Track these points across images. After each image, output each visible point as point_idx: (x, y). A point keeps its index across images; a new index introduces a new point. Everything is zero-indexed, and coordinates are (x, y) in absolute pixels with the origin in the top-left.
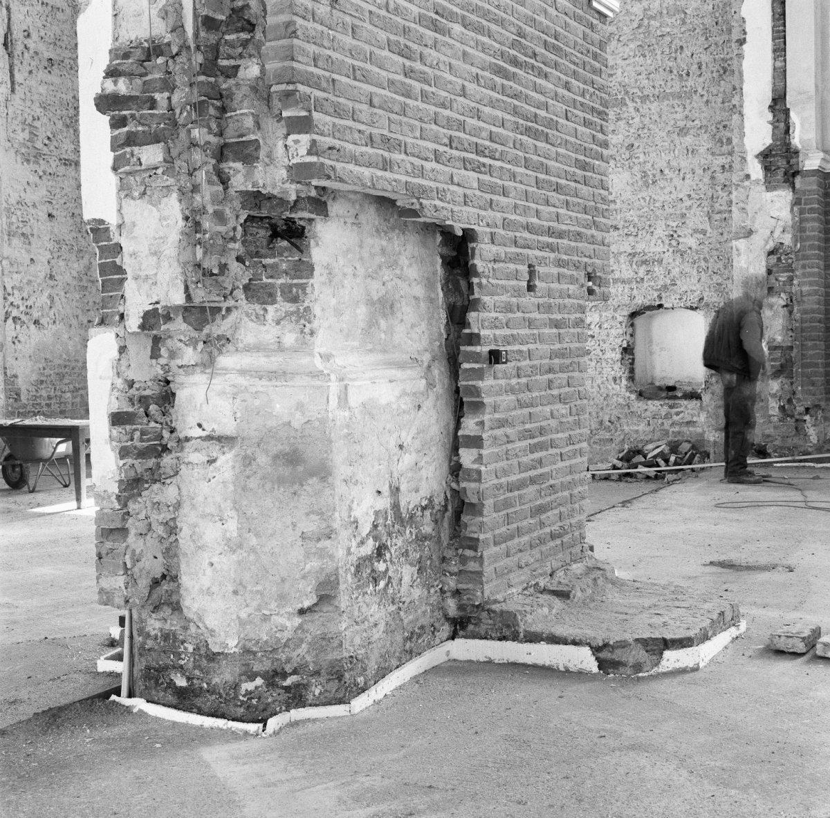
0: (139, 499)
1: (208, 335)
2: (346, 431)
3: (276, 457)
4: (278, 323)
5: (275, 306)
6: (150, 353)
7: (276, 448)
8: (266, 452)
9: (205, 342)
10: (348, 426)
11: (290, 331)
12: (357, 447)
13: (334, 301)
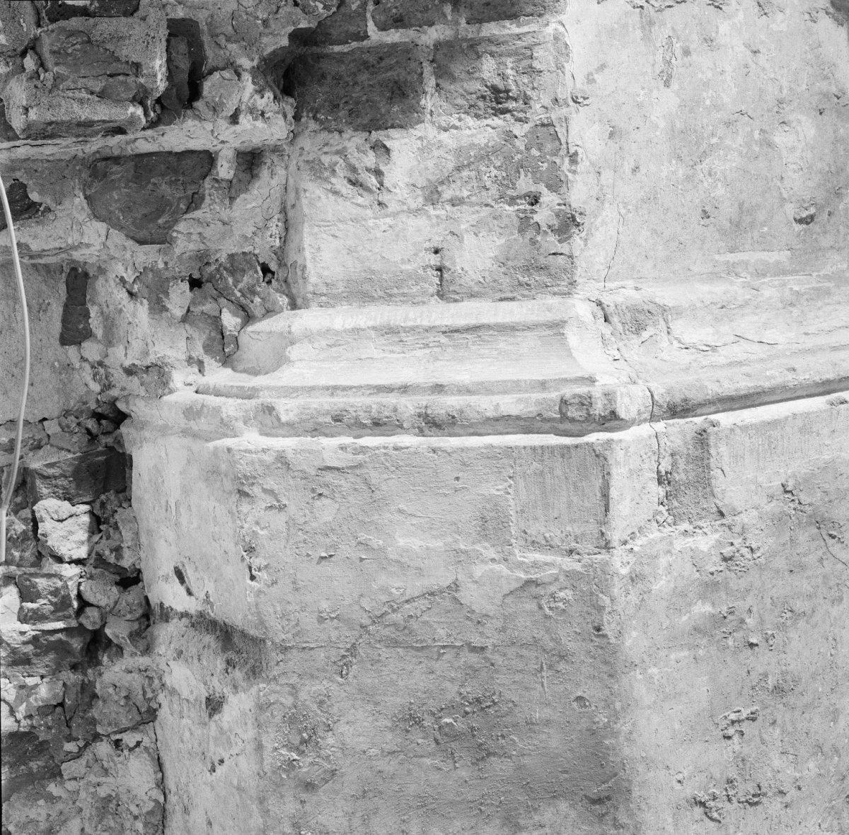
0: (53, 788)
1: (203, 258)
2: (703, 609)
3: (410, 720)
4: (432, 195)
5: (419, 131)
6: (57, 327)
7: (408, 680)
8: (368, 696)
9: (195, 284)
10: (710, 587)
11: (476, 228)
12: (763, 661)
13: (666, 103)
